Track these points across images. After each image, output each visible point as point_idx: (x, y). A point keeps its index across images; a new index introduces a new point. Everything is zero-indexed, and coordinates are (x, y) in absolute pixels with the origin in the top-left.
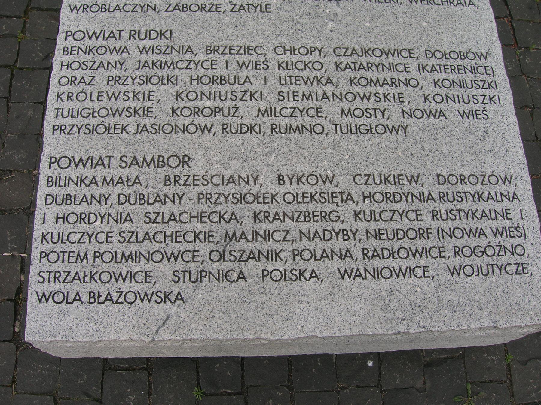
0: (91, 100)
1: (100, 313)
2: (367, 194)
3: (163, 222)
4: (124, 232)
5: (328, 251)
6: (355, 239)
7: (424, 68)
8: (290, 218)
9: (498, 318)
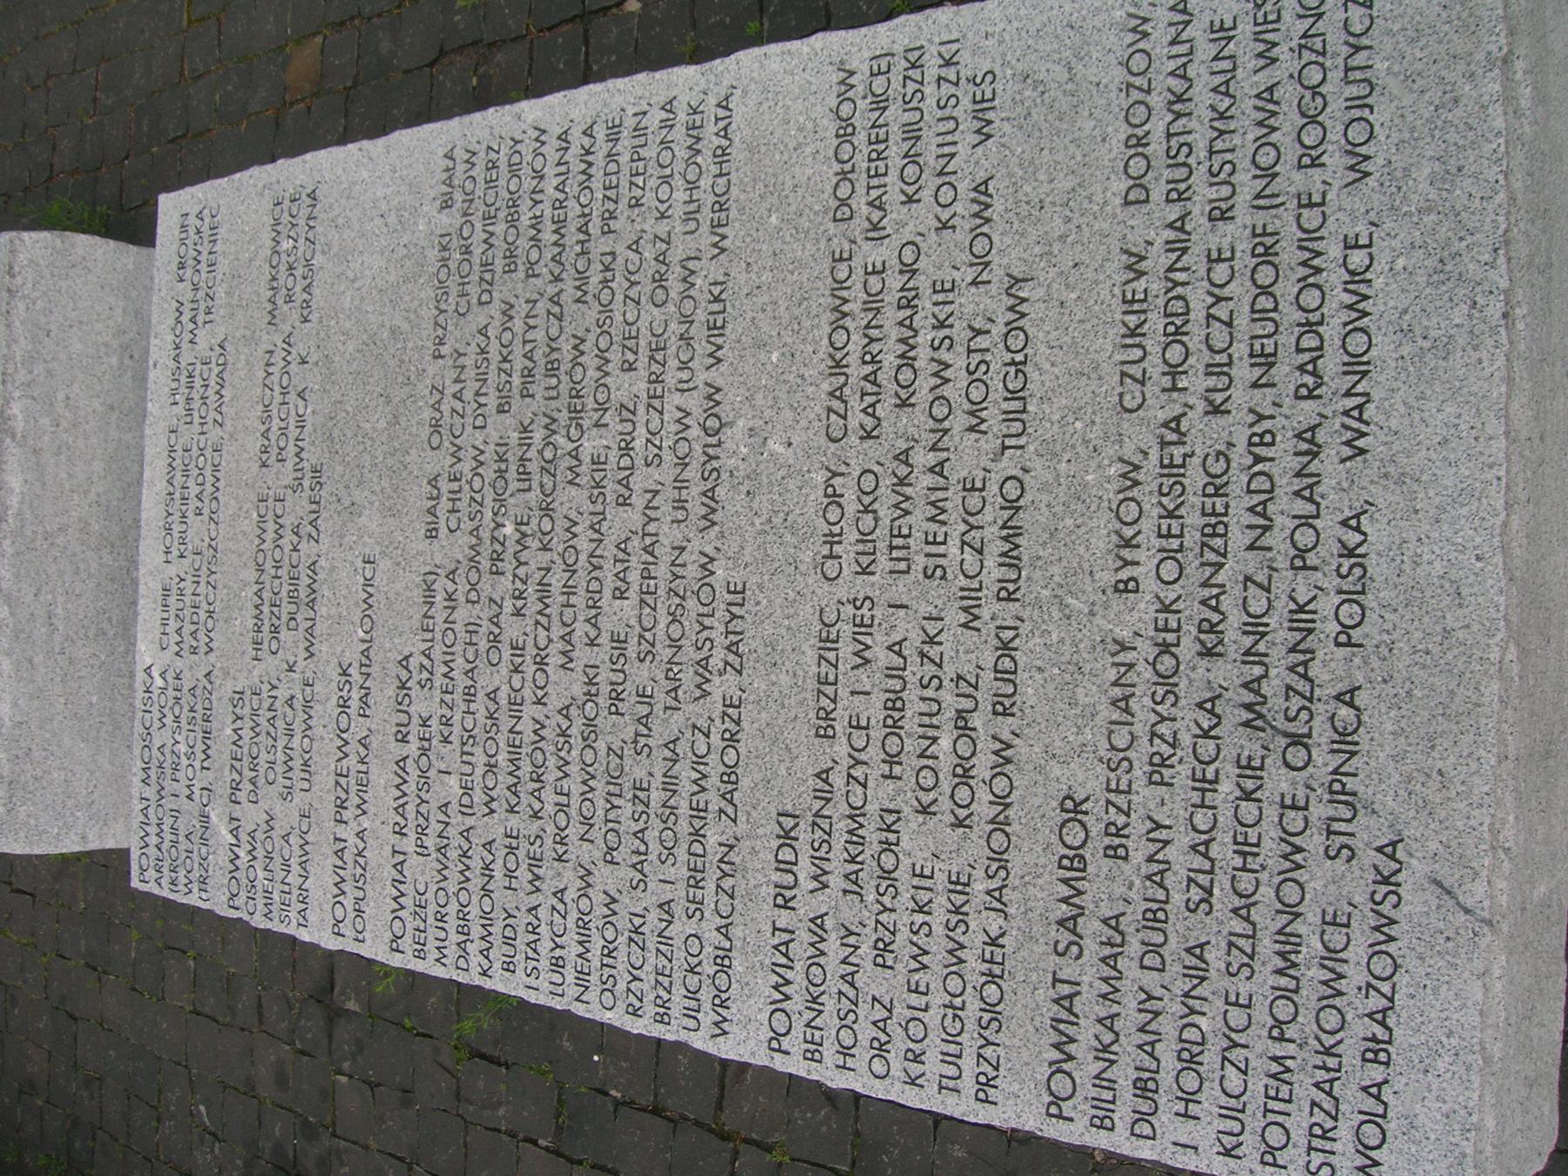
0: (925, 1010)
1: (1413, 1041)
2: (1166, 382)
3: (1211, 872)
4: (1229, 964)
5: (1298, 484)
6: (1272, 417)
7: (875, 228)
8: (1217, 572)
9: (1480, 56)
